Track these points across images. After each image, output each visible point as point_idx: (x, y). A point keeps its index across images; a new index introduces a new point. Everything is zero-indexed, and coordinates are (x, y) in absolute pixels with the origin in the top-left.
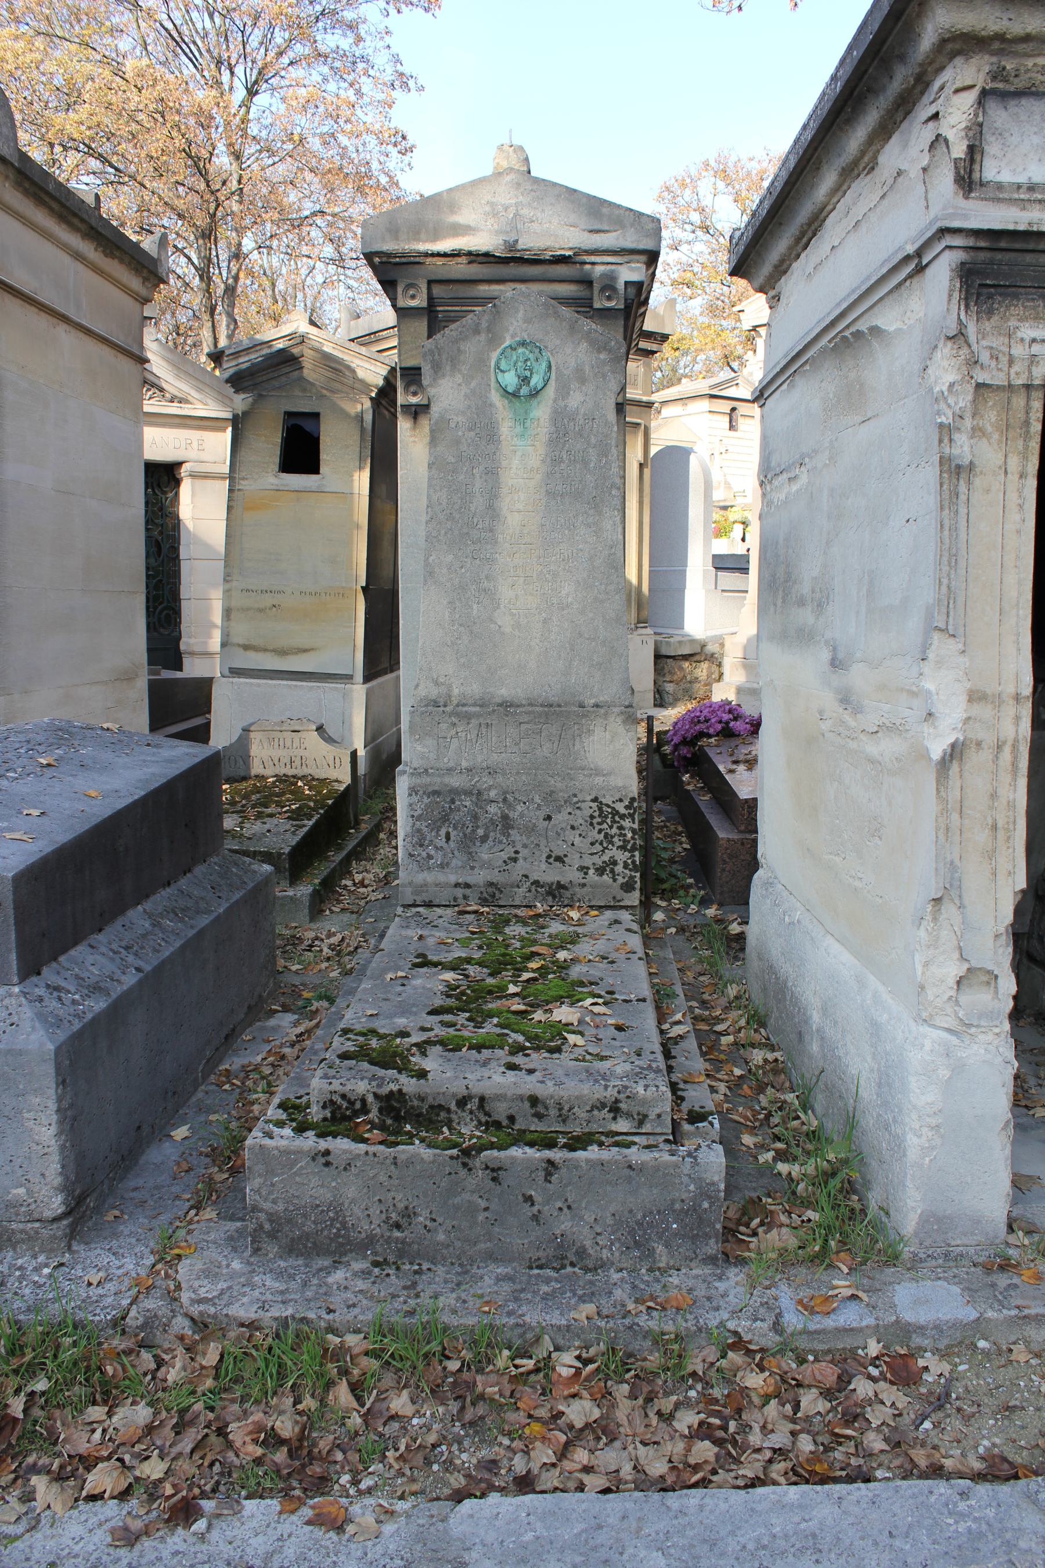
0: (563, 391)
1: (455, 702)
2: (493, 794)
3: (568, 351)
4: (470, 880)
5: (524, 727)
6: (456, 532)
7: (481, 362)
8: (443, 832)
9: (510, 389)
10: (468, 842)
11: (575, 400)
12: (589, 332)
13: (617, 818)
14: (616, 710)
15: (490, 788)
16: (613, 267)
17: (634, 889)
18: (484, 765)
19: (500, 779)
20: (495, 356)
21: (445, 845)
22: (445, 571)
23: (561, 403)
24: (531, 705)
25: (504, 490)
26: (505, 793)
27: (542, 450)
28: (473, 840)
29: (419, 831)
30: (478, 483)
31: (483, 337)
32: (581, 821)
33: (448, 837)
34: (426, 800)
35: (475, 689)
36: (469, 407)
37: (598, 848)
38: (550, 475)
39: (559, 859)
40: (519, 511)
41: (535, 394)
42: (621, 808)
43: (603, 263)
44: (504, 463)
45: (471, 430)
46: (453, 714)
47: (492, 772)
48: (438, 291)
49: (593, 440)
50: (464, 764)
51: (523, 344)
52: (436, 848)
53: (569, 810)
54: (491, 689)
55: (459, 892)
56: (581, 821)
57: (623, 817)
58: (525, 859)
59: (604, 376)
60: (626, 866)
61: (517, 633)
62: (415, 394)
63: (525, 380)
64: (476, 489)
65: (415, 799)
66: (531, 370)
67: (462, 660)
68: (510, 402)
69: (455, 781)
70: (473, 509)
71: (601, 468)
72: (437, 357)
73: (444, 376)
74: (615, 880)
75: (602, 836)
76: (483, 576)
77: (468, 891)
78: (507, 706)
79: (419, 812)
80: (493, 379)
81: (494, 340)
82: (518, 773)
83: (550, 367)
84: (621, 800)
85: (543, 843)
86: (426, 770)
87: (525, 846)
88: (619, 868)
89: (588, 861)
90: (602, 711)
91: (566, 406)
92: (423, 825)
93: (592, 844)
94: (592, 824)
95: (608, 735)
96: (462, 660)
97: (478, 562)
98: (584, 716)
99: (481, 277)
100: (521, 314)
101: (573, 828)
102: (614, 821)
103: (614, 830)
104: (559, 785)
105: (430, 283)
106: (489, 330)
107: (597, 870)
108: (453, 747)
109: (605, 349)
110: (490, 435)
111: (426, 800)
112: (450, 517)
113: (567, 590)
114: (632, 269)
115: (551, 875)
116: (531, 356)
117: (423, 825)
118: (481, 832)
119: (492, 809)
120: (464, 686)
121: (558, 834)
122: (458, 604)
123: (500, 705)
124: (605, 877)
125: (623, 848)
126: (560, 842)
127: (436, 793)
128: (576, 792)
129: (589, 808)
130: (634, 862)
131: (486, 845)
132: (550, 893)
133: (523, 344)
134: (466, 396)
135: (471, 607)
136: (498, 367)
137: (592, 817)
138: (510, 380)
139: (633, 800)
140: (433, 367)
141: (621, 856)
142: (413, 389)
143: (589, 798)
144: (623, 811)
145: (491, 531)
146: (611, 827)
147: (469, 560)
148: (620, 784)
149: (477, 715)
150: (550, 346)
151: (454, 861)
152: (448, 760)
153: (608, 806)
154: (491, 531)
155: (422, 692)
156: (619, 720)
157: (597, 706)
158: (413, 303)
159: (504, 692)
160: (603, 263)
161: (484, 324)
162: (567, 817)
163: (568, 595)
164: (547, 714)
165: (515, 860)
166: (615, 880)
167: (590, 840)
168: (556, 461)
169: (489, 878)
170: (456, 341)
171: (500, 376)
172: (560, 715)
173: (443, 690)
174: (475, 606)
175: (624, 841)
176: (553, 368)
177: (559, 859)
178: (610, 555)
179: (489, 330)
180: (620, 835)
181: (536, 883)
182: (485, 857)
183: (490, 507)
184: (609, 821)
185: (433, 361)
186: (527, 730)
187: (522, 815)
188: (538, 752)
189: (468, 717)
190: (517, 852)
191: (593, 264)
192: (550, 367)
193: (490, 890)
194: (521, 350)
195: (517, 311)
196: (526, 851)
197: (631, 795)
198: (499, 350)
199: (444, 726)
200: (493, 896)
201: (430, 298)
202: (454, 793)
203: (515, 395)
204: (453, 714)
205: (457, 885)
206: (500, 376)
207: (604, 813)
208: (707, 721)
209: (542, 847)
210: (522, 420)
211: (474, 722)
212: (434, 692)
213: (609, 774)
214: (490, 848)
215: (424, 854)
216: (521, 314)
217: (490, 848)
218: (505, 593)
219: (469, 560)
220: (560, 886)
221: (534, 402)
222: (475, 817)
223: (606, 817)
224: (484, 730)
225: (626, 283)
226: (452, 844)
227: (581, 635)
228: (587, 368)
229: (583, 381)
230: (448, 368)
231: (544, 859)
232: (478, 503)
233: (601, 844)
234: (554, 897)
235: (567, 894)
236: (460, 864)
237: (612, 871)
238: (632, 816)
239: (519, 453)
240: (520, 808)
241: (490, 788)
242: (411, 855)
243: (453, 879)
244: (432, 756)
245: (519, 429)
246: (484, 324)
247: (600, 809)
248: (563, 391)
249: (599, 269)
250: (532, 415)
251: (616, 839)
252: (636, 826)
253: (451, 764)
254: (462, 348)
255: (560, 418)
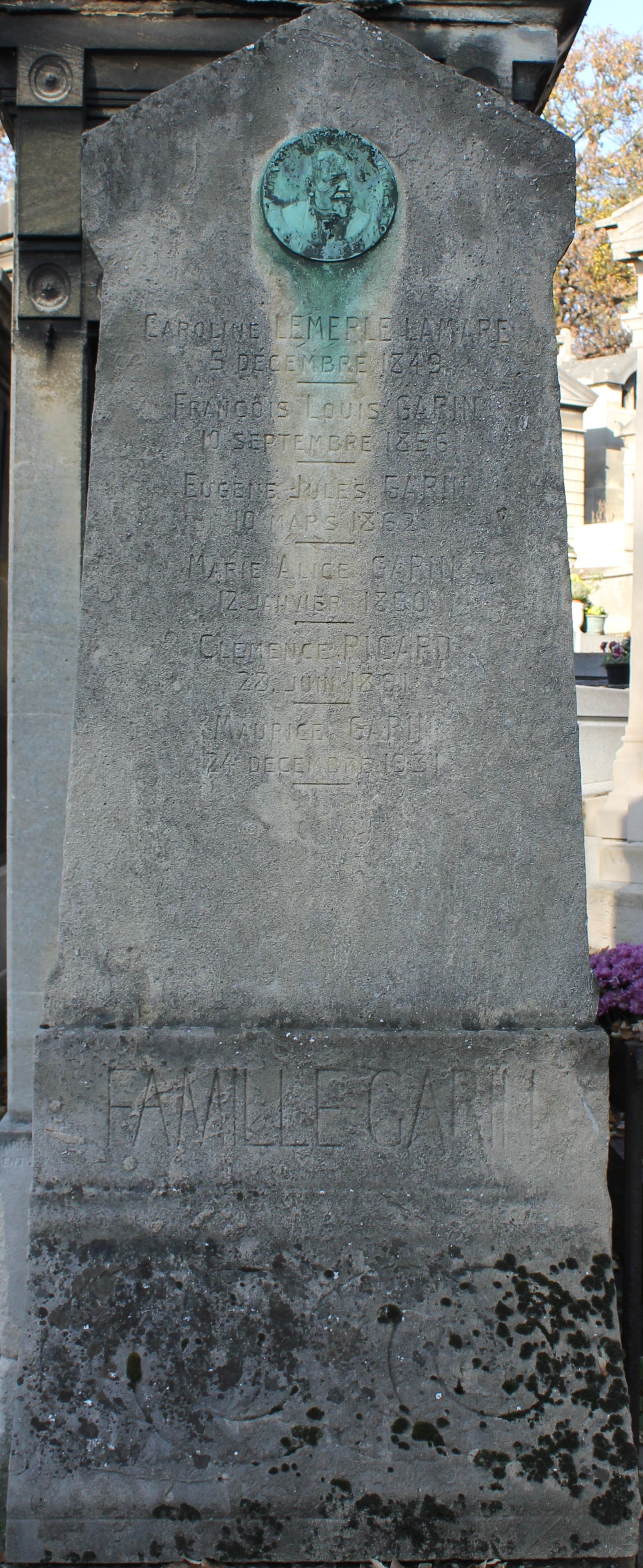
0: (427, 252)
1: (153, 1015)
2: (247, 1249)
3: (439, 158)
4: (195, 1496)
5: (326, 1080)
6: (160, 591)
7: (227, 182)
8: (121, 1358)
9: (298, 246)
10: (189, 1387)
11: (455, 274)
12: (489, 114)
13: (566, 1314)
14: (559, 1035)
15: (239, 1235)
16: (489, 32)
17: (626, 1514)
18: (226, 1175)
19: (265, 1212)
20: (260, 165)
21: (127, 1396)
22: (130, 686)
23: (422, 282)
24: (344, 1022)
25: (282, 490)
26: (279, 1246)
27: (372, 392)
28: (198, 1379)
29: (59, 1354)
30: (216, 471)
31: (232, 121)
32: (475, 1323)
33: (134, 1369)
34: (77, 1268)
35: (203, 983)
36: (197, 286)
37: (524, 1398)
38: (392, 454)
39: (427, 1433)
40: (317, 542)
41: (358, 257)
42: (572, 1284)
43: (467, 23)
44: (281, 425)
45: (199, 341)
46: (142, 1047)
47: (245, 1192)
48: (106, 73)
49: (499, 371)
50: (175, 1173)
51: (330, 138)
52: (104, 1402)
53: (444, 1292)
54: (245, 984)
55: (167, 1530)
56: (475, 1323)
57: (580, 1309)
58: (338, 1433)
59: (525, 220)
60: (601, 1451)
61: (309, 842)
62: (51, 294)
63: (335, 225)
64: (212, 486)
65: (48, 1263)
66: (348, 201)
67: (172, 910)
68: (298, 275)
69: (152, 1218)
70: (202, 534)
71: (519, 438)
72: (118, 164)
73: (135, 210)
74: (576, 1492)
75: (532, 1363)
76: (225, 700)
77: (190, 1528)
78: (284, 1026)
79: (59, 1300)
80: (255, 231)
81: (259, 129)
82: (312, 1196)
83: (393, 195)
84: (572, 1264)
85: (382, 1387)
86: (78, 1189)
87: (336, 1396)
88: (584, 1456)
89: (503, 1438)
90: (524, 1038)
91: (433, 289)
92: (67, 1337)
93: (510, 1387)
94: (503, 1331)
95: (537, 1100)
96: (172, 910)
97: (213, 664)
98: (477, 1051)
99: (201, 45)
100: (324, 70)
101: (456, 1342)
102: (559, 1323)
103: (562, 1349)
104: (415, 1225)
105: (90, 55)
106: (247, 103)
107: (526, 1462)
108: (146, 1129)
109: (526, 156)
110: (249, 354)
111: (77, 1268)
112: (146, 554)
113: (435, 735)
114: (529, 37)
115: (406, 1479)
116: (349, 167)
117: (67, 1337)
118: (219, 1356)
119: (247, 1291)
120: (175, 976)
121: (420, 1361)
122: (161, 769)
123: (266, 1023)
124: (550, 1483)
125: (587, 1397)
126: (426, 1384)
127: (103, 1248)
128: (459, 1241)
129: (493, 1286)
130: (620, 1437)
131: (236, 1395)
132: (409, 1529)
133: (330, 138)
134: (189, 259)
135: (194, 777)
136: (267, 191)
137: (503, 1311)
138: (297, 222)
139: (601, 1261)
140: (108, 189)
141: (588, 1422)
142: (46, 283)
143: (491, 1259)
144: (579, 1293)
145: (247, 588)
146: (553, 1339)
147: (191, 661)
148: (569, 1223)
149: (210, 1050)
150: (396, 145)
151: (153, 1441)
152: (135, 1162)
153: (541, 1280)
154: (247, 588)
155: (69, 989)
156: (566, 1060)
157: (508, 1024)
158: (52, 97)
159: (274, 991)
160: (467, 23)
161: (236, 91)
162: (439, 1312)
163: (437, 750)
164: (385, 1048)
165: (312, 1436)
166: (576, 1492)
167: (503, 1375)
168: (407, 421)
169: (246, 1491)
170: (169, 128)
171: (273, 213)
172: (420, 1047)
173: (122, 984)
174: (205, 776)
175: (591, 1377)
176: (403, 198)
177: (427, 1433)
178: (541, 650)
179: (247, 103)
180: (579, 1360)
181: (371, 1503)
182: (234, 1427)
183: (246, 530)
184: (546, 1320)
185: (109, 175)
186: (335, 1087)
187: (324, 1308)
188: (363, 1143)
189: (184, 1055)
190: (315, 1414)
191: (446, 23)
192: (393, 195)
193: (249, 1523)
194: (324, 153)
195: (316, 62)
196: (339, 1410)
197: (595, 1250)
198: (271, 153)
199: (123, 1076)
200: (257, 1538)
201: (90, 89)
202: (150, 1248)
203: (309, 260)
204: (142, 1047)
205: (161, 1511)
206: (273, 213)
207: (531, 1300)
208: (625, 985)
209: (381, 1398)
210: (326, 319)
211: (202, 1067)
212: (100, 990)
213: (541, 1197)
214: (246, 1403)
215: (73, 1422)
216: (324, 70)
217: (246, 1403)
218: (281, 742)
219: (191, 661)
220: (434, 1509)
221: (356, 278)
222: (204, 1315)
223: (538, 1310)
224: (226, 1088)
225: (517, 65)
226: (146, 1393)
227: (468, 848)
228: (484, 201)
229: (473, 228)
230: (146, 192)
231: (387, 1435)
232: (216, 520)
233: (532, 1386)
234: (418, 1540)
235: (453, 1531)
236: (167, 1449)
237: (567, 1465)
238: (601, 1305)
239: (318, 401)
240: (317, 1288)
241: (239, 1235)
242: (38, 1425)
243: (149, 1493)
244: (94, 1153)
245: (318, 342)
246: (236, 91)
247: (522, 1289)
248: (427, 252)
249: (458, 35)
250: (349, 309)
251: (568, 1373)
252: (615, 1335)
253: (142, 1174)
254: (181, 145)
255: (419, 317)
